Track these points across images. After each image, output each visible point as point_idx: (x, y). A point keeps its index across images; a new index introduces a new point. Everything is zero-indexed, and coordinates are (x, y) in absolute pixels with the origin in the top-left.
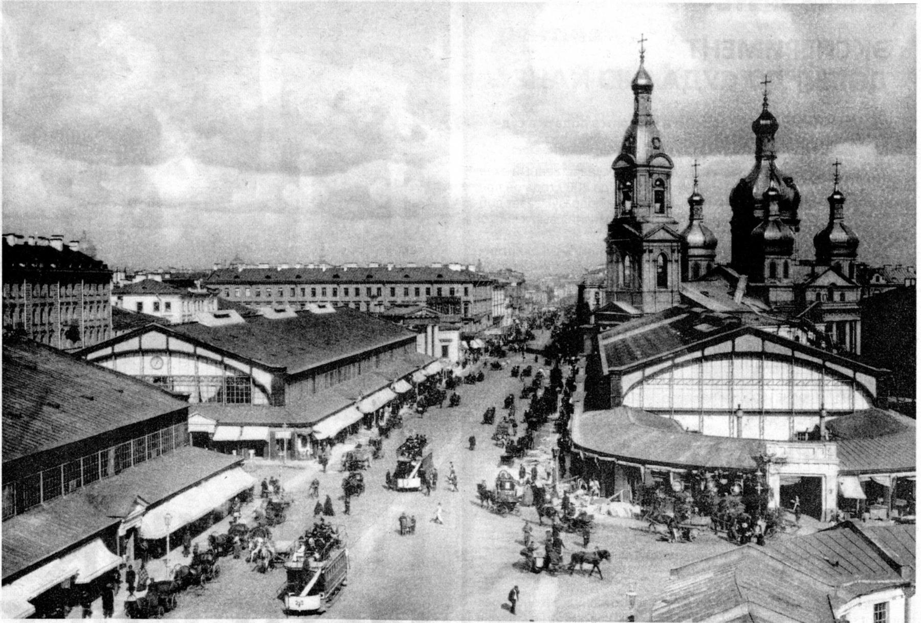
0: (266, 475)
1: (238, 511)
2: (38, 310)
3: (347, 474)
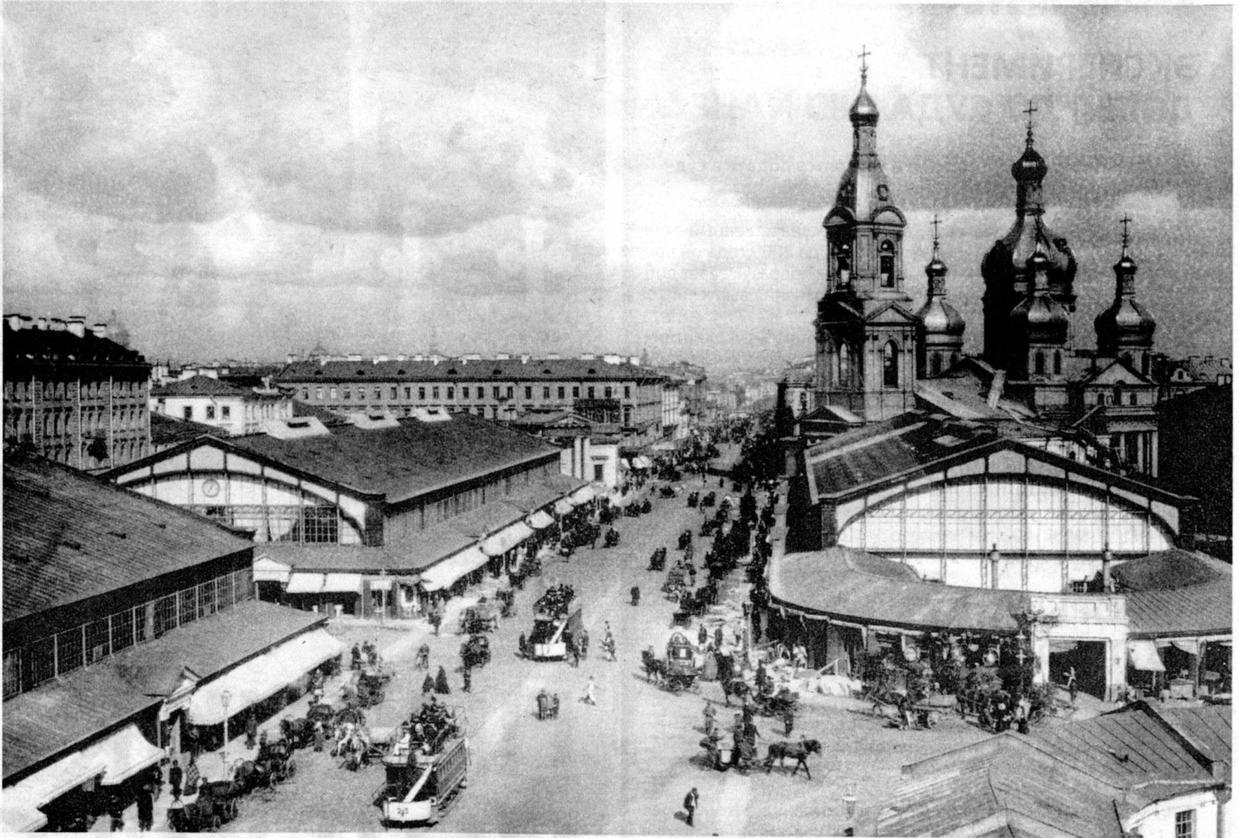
0: (358, 639)
1: (321, 687)
2: (52, 416)
3: (466, 638)
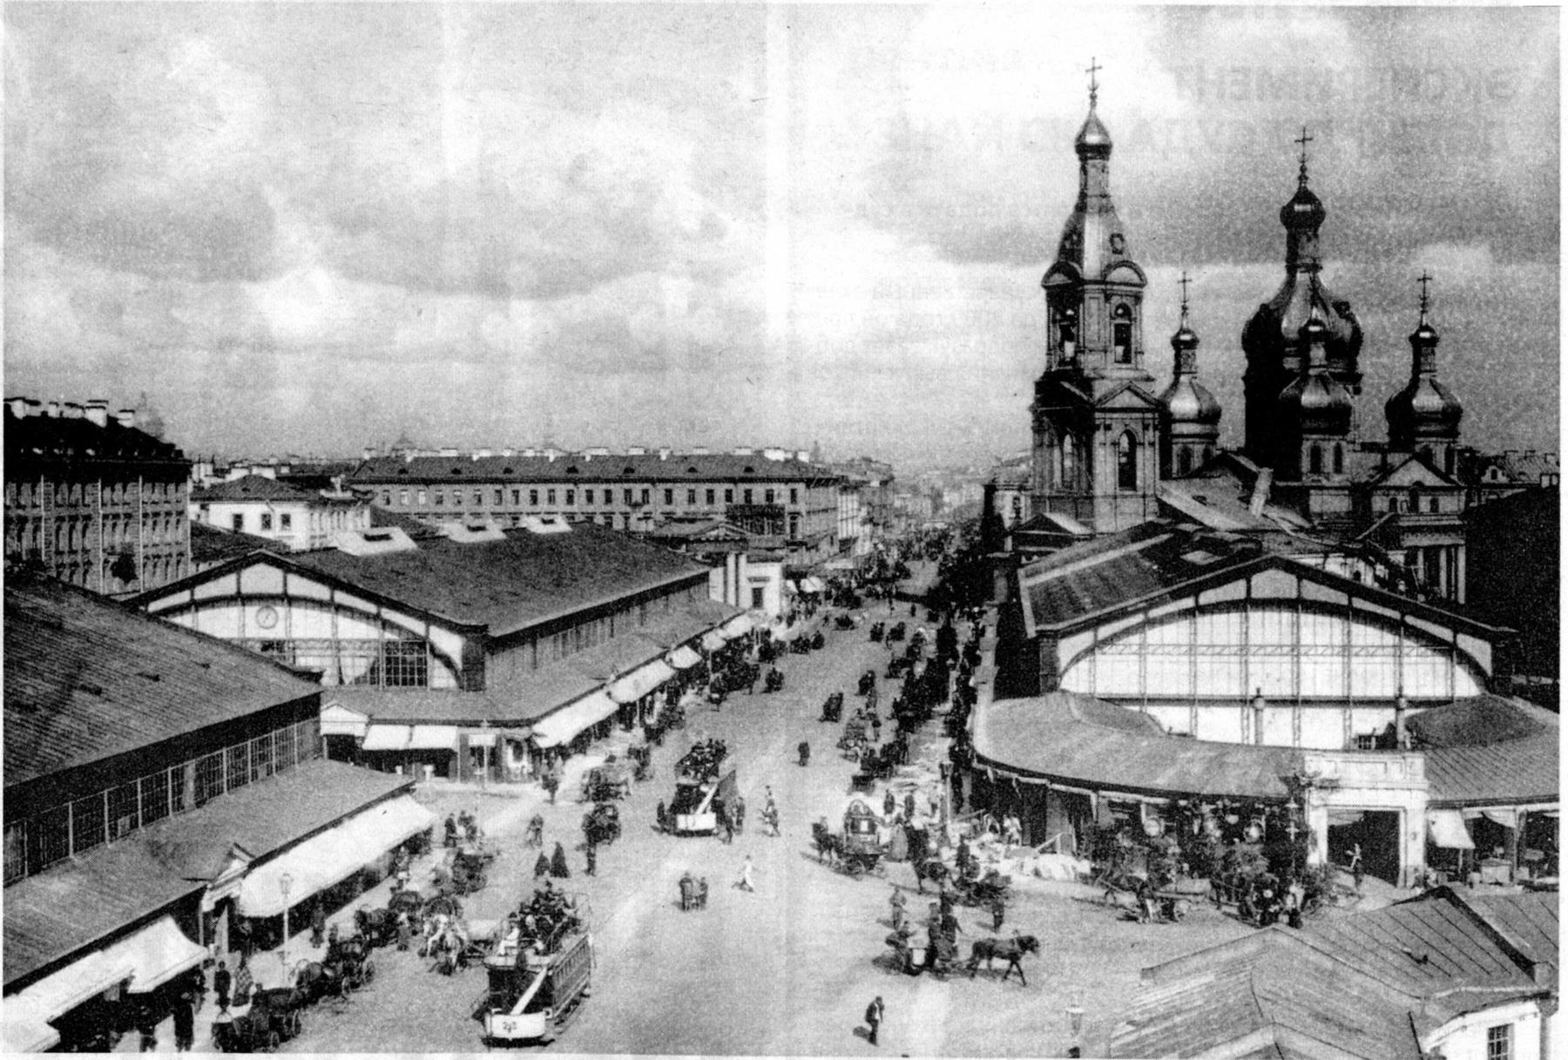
0: (454, 808)
1: (406, 869)
2: (65, 527)
3: (590, 807)
